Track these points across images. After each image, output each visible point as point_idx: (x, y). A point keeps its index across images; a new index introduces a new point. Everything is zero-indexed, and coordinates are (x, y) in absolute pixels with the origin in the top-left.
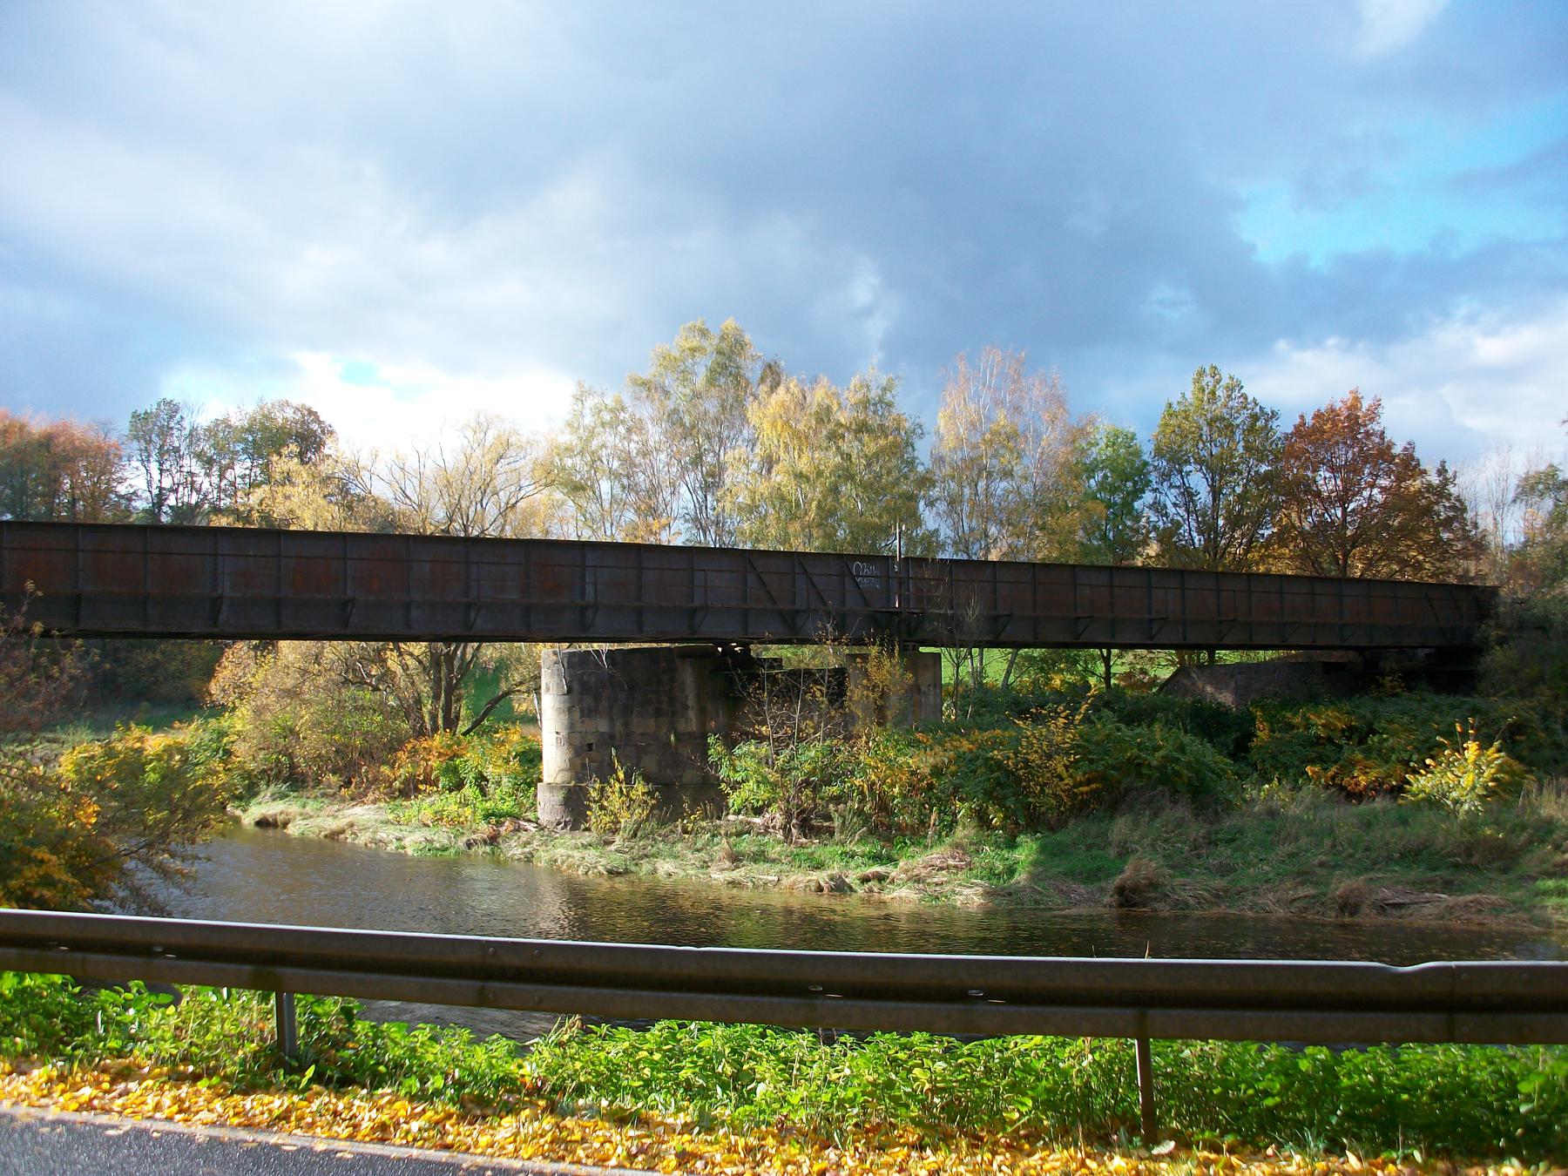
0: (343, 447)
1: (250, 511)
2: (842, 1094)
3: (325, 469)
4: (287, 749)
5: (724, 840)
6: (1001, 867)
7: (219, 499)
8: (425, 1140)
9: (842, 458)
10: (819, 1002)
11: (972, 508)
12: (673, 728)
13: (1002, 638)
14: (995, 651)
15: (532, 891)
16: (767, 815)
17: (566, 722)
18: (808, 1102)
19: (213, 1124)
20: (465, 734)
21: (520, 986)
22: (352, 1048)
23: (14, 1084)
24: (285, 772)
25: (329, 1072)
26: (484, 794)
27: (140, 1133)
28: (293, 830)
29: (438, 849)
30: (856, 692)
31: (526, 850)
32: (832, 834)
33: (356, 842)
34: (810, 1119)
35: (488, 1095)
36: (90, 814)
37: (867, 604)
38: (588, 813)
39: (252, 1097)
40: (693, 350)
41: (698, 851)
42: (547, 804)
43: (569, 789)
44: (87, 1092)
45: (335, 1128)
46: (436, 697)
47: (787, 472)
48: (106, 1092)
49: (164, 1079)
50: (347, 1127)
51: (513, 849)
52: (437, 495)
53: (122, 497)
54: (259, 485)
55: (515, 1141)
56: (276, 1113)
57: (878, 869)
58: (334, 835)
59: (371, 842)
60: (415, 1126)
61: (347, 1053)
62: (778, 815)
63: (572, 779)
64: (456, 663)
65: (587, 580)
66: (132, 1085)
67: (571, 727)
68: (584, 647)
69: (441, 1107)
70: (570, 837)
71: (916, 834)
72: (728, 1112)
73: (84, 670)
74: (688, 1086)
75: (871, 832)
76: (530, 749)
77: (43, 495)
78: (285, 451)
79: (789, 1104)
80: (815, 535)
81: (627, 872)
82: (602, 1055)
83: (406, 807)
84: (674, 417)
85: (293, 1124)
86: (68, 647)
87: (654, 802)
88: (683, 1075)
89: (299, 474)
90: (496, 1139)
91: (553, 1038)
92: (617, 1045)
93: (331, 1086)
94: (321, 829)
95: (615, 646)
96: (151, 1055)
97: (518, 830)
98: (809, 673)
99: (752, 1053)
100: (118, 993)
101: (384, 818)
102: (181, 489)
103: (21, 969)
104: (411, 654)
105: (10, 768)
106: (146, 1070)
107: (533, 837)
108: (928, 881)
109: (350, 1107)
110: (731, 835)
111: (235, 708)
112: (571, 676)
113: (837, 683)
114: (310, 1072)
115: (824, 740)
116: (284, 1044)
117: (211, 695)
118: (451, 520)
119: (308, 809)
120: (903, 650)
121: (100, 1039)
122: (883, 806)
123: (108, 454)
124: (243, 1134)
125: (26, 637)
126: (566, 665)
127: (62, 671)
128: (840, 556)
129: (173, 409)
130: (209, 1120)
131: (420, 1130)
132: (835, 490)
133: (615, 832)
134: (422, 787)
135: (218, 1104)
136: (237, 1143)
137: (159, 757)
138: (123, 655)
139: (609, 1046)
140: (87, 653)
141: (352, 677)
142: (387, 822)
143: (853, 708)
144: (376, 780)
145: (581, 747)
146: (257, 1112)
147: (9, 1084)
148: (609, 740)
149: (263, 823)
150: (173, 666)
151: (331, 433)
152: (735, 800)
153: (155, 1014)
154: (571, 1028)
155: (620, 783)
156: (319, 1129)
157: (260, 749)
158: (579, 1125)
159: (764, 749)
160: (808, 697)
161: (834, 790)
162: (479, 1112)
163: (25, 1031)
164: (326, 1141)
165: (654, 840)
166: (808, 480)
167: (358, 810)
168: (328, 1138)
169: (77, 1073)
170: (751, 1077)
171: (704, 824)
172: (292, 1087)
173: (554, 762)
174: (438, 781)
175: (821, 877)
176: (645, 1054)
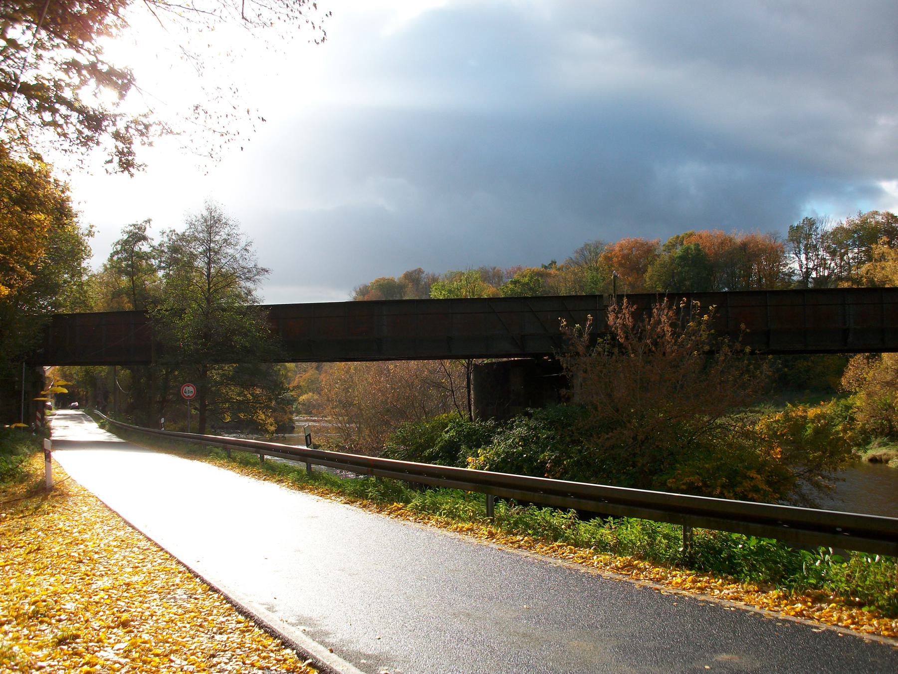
1: (861, 278)
7: (841, 272)
19: (873, 633)
23: (760, 597)
24: (886, 431)
28: (892, 464)
36: (777, 453)
44: (799, 606)
49: (842, 604)
53: (786, 274)
54: (864, 263)
66: (823, 605)
89: (889, 253)
100: (814, 554)
103: (760, 535)
105: (735, 426)
106: (832, 597)
111: (856, 393)
117: (842, 385)
121: (804, 577)
123: (777, 251)
125: (742, 354)
127: (761, 373)
129: (811, 223)
135: (875, 622)
137: (813, 421)
147: (757, 597)
149: (874, 460)
157: (871, 417)
163: (763, 570)
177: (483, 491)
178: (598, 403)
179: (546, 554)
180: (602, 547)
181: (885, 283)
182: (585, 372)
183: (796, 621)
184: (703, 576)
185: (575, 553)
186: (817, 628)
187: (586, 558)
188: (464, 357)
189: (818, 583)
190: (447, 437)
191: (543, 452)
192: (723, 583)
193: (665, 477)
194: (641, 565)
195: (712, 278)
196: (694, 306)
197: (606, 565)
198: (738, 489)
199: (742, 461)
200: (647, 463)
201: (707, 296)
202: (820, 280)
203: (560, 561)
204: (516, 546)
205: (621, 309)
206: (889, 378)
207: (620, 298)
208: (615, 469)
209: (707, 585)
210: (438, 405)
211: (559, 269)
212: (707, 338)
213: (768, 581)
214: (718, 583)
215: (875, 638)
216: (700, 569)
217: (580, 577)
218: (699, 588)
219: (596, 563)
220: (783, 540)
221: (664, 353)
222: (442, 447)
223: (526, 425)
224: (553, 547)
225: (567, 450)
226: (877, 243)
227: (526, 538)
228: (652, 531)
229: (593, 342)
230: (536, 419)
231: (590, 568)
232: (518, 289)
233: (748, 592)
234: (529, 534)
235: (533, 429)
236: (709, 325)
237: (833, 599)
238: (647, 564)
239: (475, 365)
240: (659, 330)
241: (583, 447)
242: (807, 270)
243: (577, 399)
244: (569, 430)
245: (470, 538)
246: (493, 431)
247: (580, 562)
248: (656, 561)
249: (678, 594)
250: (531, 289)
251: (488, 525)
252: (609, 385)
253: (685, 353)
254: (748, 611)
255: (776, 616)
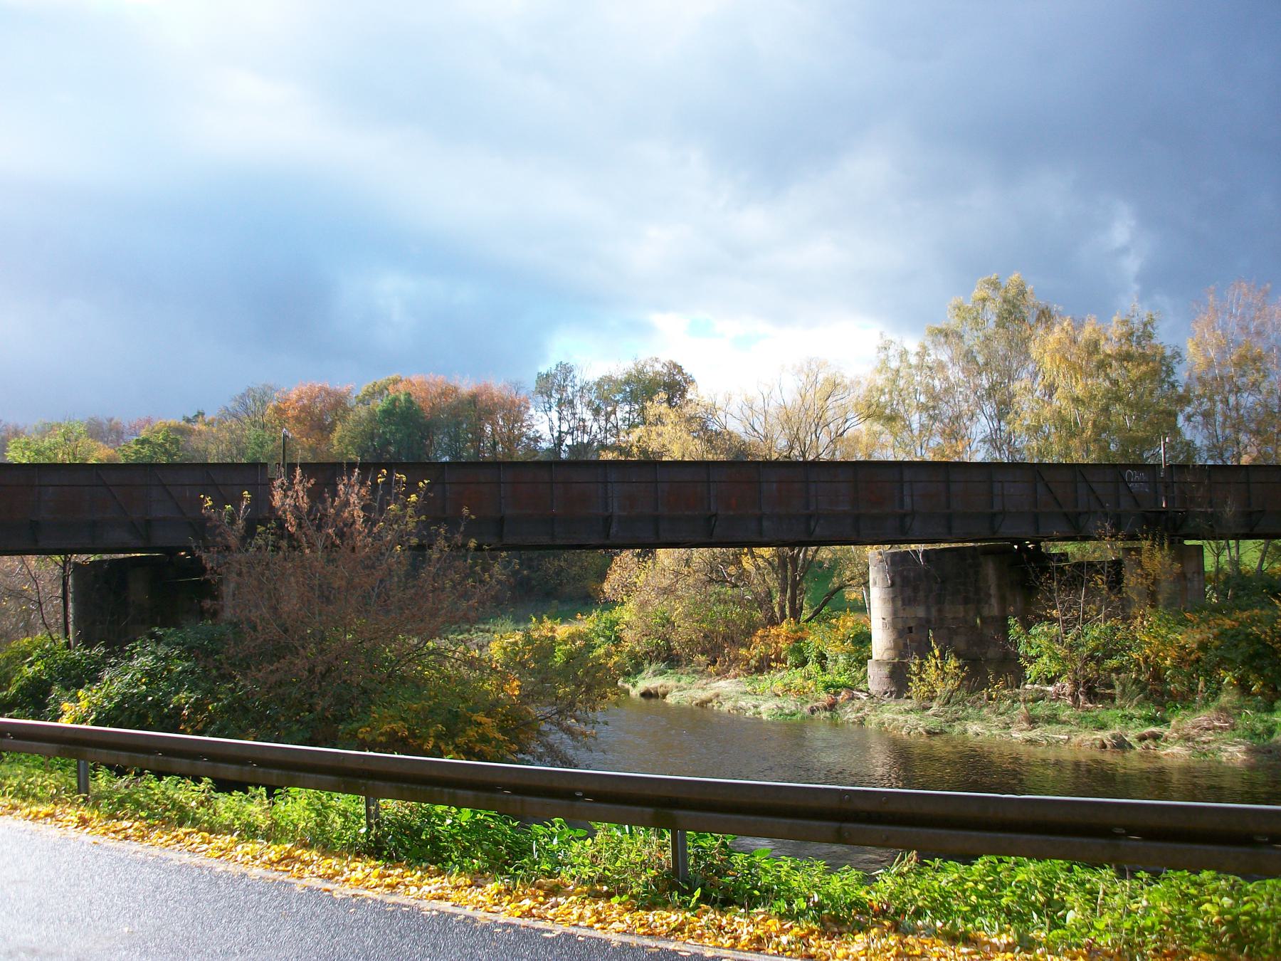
0: (702, 392)
1: (631, 446)
2: (1142, 923)
3: (688, 411)
4: (665, 636)
5: (1022, 706)
6: (1261, 728)
8: (792, 951)
9: (1111, 383)
10: (1122, 843)
11: (1225, 420)
12: (978, 613)
13: (1256, 530)
14: (1250, 543)
15: (863, 747)
16: (1058, 685)
17: (890, 610)
18: (1116, 928)
20: (807, 621)
21: (870, 827)
22: (732, 876)
23: (473, 894)
25: (714, 895)
26: (824, 668)
27: (570, 936)
28: (670, 700)
29: (787, 715)
30: (1131, 580)
31: (859, 715)
32: (1113, 700)
33: (721, 709)
34: (1114, 944)
35: (843, 916)
36: (514, 688)
37: (1137, 504)
38: (910, 684)
39: (654, 912)
40: (984, 300)
41: (1001, 714)
42: (876, 677)
43: (894, 665)
45: (720, 939)
46: (784, 591)
47: (1066, 398)
48: (541, 904)
49: (585, 895)
50: (729, 939)
51: (849, 714)
52: (779, 428)
53: (531, 439)
54: (637, 426)
55: (866, 954)
56: (673, 925)
57: (1153, 729)
58: (703, 704)
59: (733, 709)
60: (784, 939)
61: (728, 880)
62: (1067, 684)
63: (896, 657)
64: (800, 562)
65: (905, 493)
66: (561, 900)
67: (895, 614)
68: (904, 548)
69: (806, 924)
70: (895, 704)
71: (1185, 700)
72: (1043, 934)
73: (508, 576)
74: (1008, 912)
75: (1146, 698)
76: (861, 632)
77: (472, 441)
78: (656, 398)
79: (1096, 929)
80: (1092, 448)
81: (942, 732)
82: (935, 884)
83: (761, 681)
84: (969, 356)
85: (686, 935)
86: (494, 558)
87: (964, 674)
88: (1004, 901)
90: (850, 952)
91: (895, 869)
92: (947, 876)
93: (716, 905)
94: (693, 699)
95: (929, 547)
96: (574, 877)
97: (852, 698)
98: (1091, 564)
99: (1061, 885)
100: (548, 827)
101: (743, 689)
102: (575, 432)
103: (475, 807)
104: (762, 557)
105: (454, 652)
106: (571, 887)
107: (864, 704)
108: (1197, 739)
109: (731, 923)
110: (1029, 701)
111: (623, 603)
112: (894, 572)
113: (1115, 573)
114: (698, 893)
115: (1106, 621)
116: (678, 873)
118: (792, 448)
119: (682, 683)
120: (1171, 543)
121: (535, 862)
122: (1157, 675)
124: (647, 941)
126: (889, 562)
127: (491, 577)
128: (1114, 466)
130: (621, 929)
131: (788, 943)
132: (1106, 410)
133: (932, 699)
134: (773, 664)
135: (627, 916)
136: (643, 947)
137: (565, 642)
138: (535, 563)
139: (940, 876)
140: (509, 562)
141: (715, 577)
142: (745, 693)
143: (1129, 593)
144: (736, 659)
145: (903, 630)
146: (658, 924)
147: (470, 894)
148: (926, 624)
149: (647, 695)
150: (575, 570)
151: (693, 381)
152: (1032, 671)
153: (576, 845)
154: (909, 861)
155: (936, 658)
156: (707, 939)
158: (919, 942)
159: (1056, 629)
160: (1091, 585)
161: (1113, 663)
162: (836, 930)
163: (479, 855)
164: (713, 949)
165: (964, 705)
166: (1084, 403)
167: (723, 683)
168: (714, 947)
169: (519, 888)
170: (1062, 905)
171: (1006, 692)
172: (684, 905)
173: (881, 642)
174: (787, 659)
175: (1105, 735)
176: (971, 884)
177: (71, 757)
178: (258, 621)
179: (167, 846)
180: (250, 832)
181: (662, 455)
182: (240, 574)
183: (522, 924)
184: (395, 868)
185: (209, 843)
186: (550, 931)
187: (226, 849)
188: (58, 552)
189: (553, 869)
190: (28, 672)
191: (177, 693)
192: (422, 876)
193: (355, 725)
194: (306, 856)
195: (428, 442)
196: (398, 482)
197: (254, 858)
198: (459, 740)
199: (465, 700)
200: (330, 706)
201: (417, 467)
202: (576, 449)
203: (187, 856)
204: (121, 836)
205: (292, 483)
206: (666, 583)
207: (291, 467)
208: (283, 715)
209: (399, 880)
210: (17, 624)
211: (208, 424)
212: (415, 528)
213: (486, 870)
214: (415, 877)
215: (626, 939)
216: (390, 858)
217: (215, 880)
218: (388, 886)
219: (240, 855)
220: (506, 813)
221: (353, 549)
222: (21, 689)
223: (152, 653)
224: (176, 836)
225: (213, 689)
226: (652, 400)
227: (137, 824)
228: (322, 805)
229: (250, 531)
230: (168, 644)
231: (232, 865)
232: (146, 451)
233: (457, 887)
234: (141, 818)
235: (162, 659)
236: (418, 510)
237: (573, 890)
238: (315, 854)
239: (76, 564)
240: (346, 515)
241: (236, 684)
242: (560, 435)
243: (228, 614)
244: (215, 660)
245: (49, 831)
246: (100, 664)
247: (217, 855)
248: (327, 849)
249: (357, 895)
250: (166, 452)
251: (79, 806)
252: (274, 595)
253: (384, 547)
254: (455, 915)
255: (494, 919)
